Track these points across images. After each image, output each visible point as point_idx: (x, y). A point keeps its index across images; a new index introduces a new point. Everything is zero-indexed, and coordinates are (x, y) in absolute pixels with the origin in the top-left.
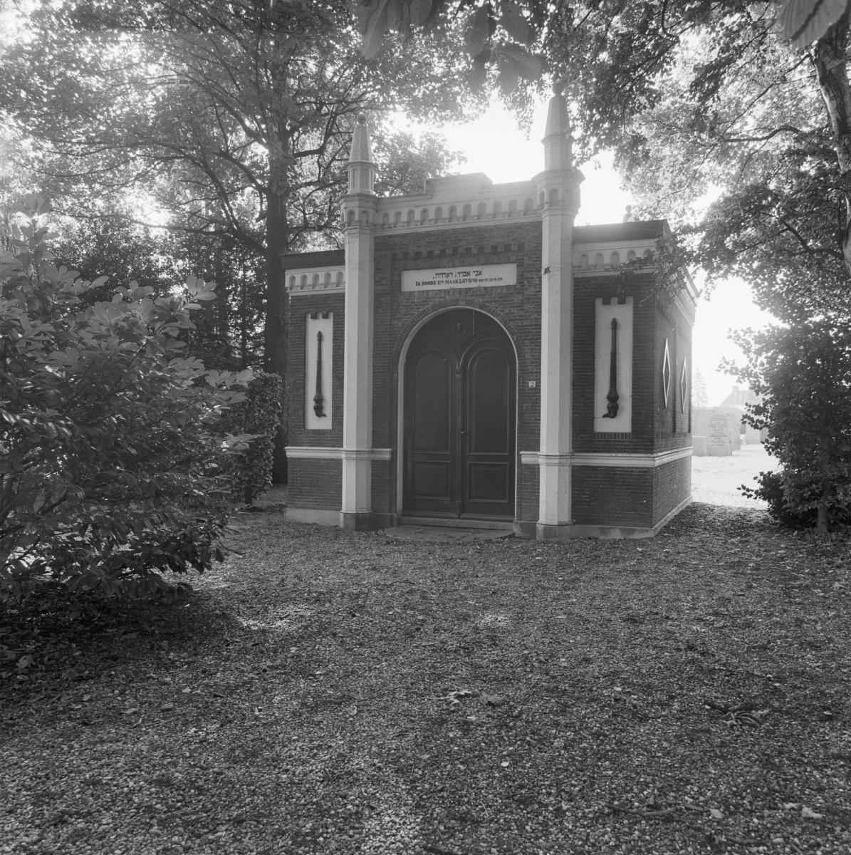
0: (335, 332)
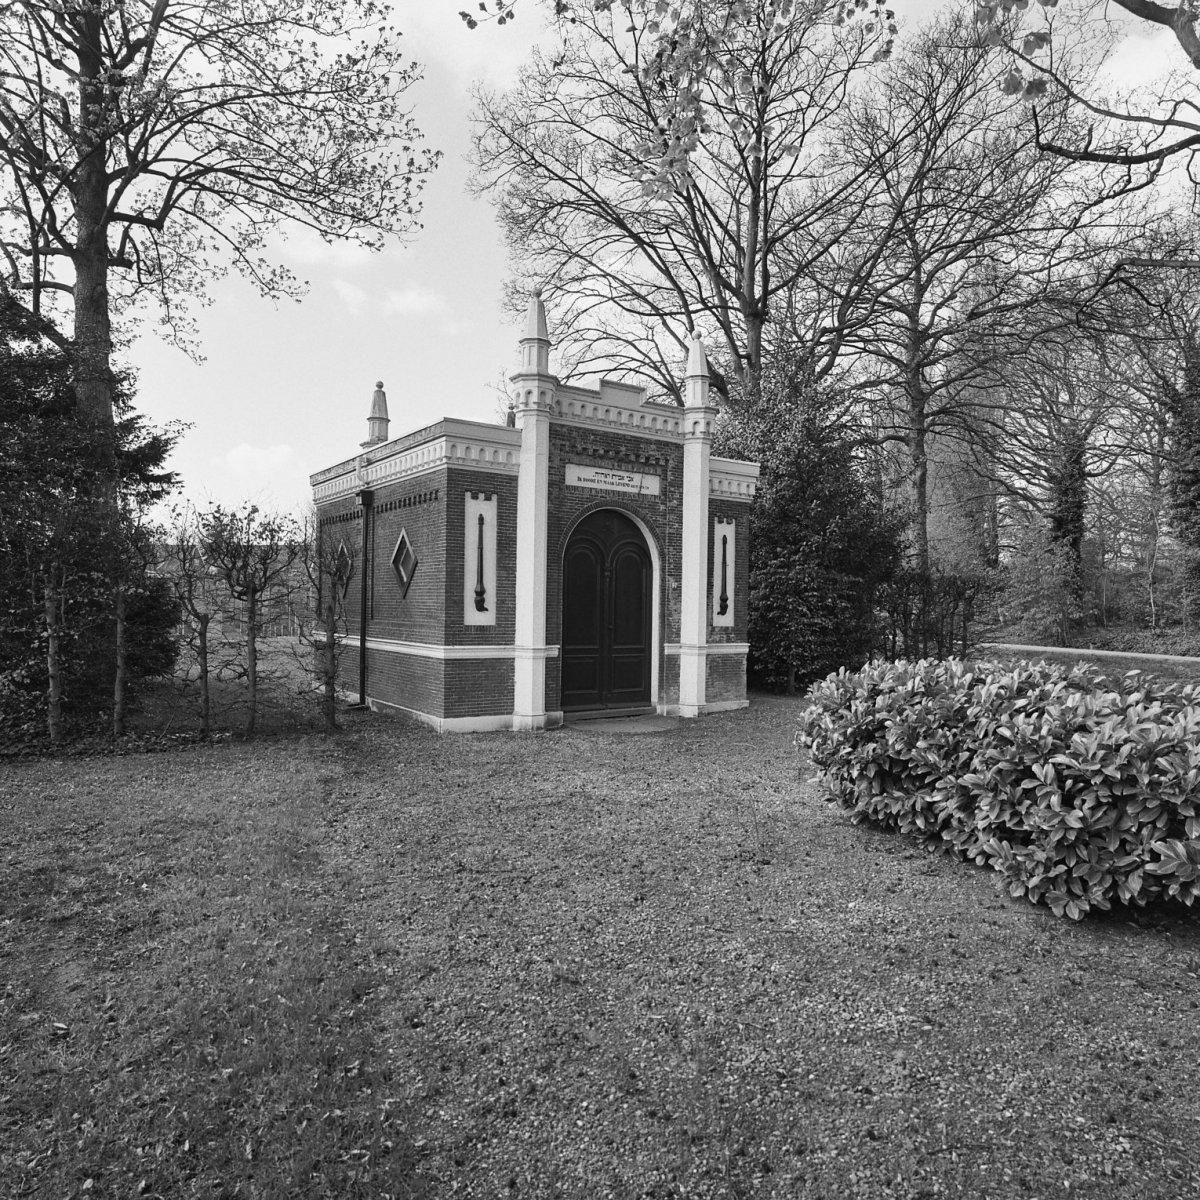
0: (500, 516)
